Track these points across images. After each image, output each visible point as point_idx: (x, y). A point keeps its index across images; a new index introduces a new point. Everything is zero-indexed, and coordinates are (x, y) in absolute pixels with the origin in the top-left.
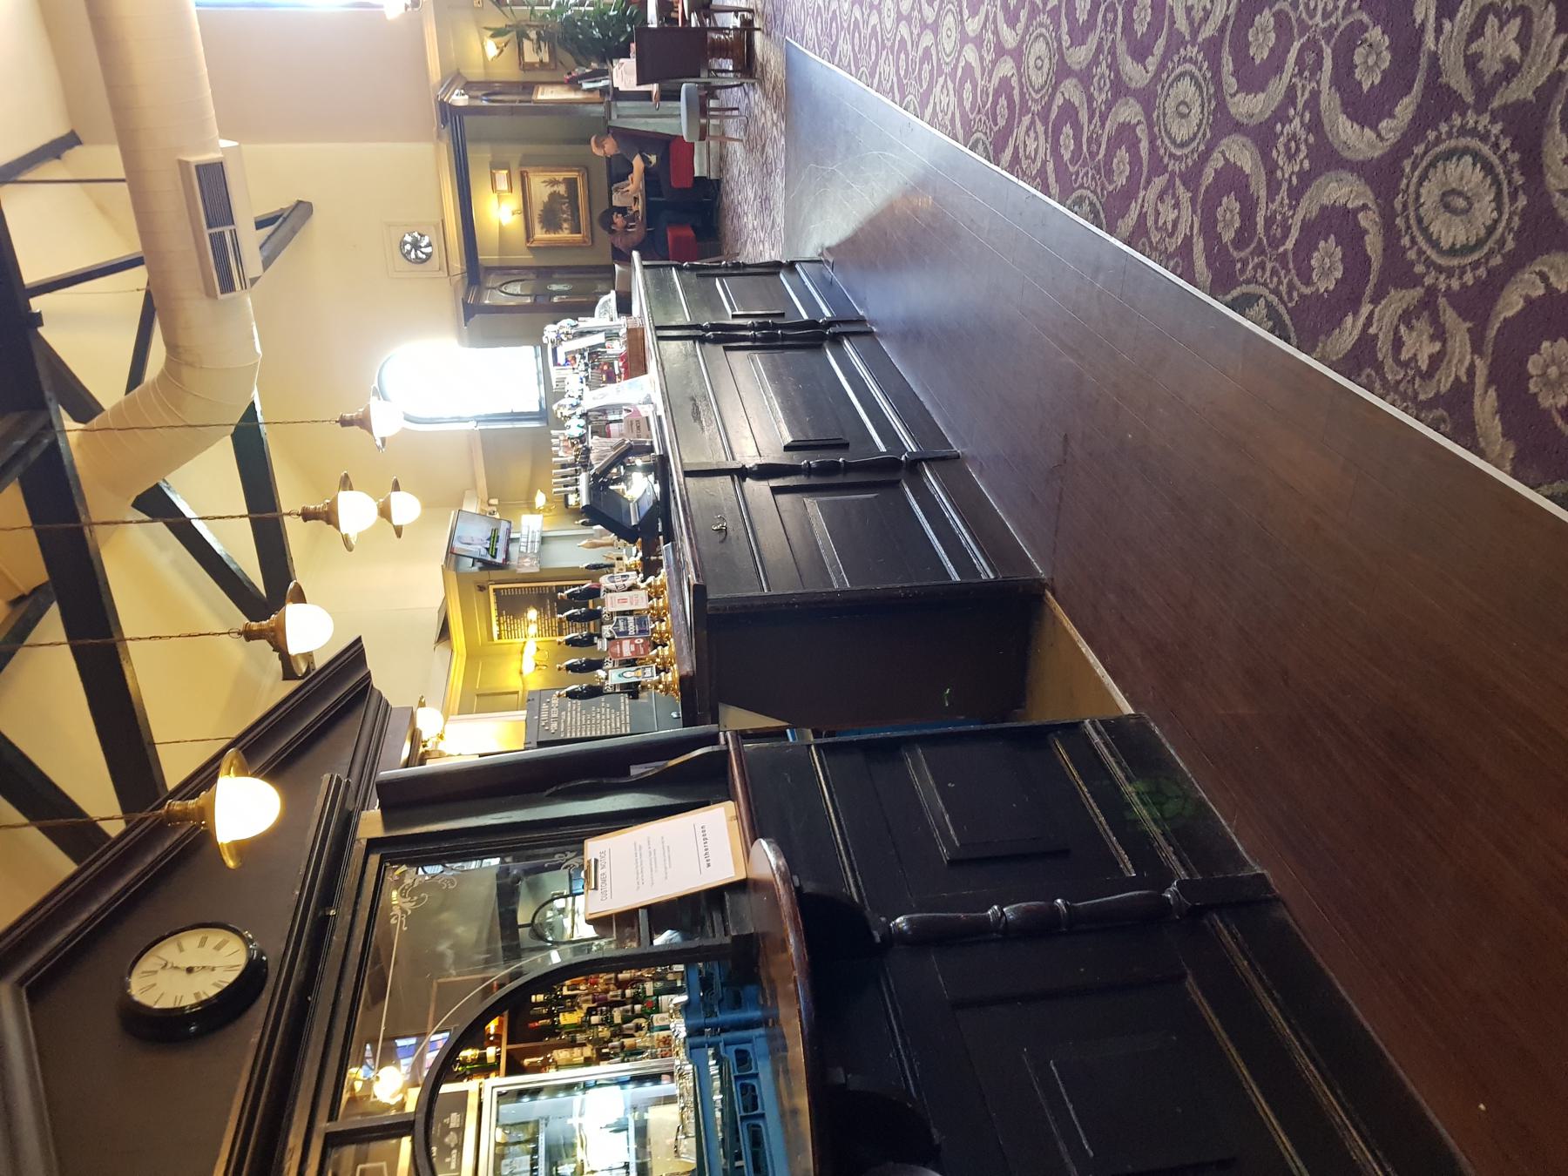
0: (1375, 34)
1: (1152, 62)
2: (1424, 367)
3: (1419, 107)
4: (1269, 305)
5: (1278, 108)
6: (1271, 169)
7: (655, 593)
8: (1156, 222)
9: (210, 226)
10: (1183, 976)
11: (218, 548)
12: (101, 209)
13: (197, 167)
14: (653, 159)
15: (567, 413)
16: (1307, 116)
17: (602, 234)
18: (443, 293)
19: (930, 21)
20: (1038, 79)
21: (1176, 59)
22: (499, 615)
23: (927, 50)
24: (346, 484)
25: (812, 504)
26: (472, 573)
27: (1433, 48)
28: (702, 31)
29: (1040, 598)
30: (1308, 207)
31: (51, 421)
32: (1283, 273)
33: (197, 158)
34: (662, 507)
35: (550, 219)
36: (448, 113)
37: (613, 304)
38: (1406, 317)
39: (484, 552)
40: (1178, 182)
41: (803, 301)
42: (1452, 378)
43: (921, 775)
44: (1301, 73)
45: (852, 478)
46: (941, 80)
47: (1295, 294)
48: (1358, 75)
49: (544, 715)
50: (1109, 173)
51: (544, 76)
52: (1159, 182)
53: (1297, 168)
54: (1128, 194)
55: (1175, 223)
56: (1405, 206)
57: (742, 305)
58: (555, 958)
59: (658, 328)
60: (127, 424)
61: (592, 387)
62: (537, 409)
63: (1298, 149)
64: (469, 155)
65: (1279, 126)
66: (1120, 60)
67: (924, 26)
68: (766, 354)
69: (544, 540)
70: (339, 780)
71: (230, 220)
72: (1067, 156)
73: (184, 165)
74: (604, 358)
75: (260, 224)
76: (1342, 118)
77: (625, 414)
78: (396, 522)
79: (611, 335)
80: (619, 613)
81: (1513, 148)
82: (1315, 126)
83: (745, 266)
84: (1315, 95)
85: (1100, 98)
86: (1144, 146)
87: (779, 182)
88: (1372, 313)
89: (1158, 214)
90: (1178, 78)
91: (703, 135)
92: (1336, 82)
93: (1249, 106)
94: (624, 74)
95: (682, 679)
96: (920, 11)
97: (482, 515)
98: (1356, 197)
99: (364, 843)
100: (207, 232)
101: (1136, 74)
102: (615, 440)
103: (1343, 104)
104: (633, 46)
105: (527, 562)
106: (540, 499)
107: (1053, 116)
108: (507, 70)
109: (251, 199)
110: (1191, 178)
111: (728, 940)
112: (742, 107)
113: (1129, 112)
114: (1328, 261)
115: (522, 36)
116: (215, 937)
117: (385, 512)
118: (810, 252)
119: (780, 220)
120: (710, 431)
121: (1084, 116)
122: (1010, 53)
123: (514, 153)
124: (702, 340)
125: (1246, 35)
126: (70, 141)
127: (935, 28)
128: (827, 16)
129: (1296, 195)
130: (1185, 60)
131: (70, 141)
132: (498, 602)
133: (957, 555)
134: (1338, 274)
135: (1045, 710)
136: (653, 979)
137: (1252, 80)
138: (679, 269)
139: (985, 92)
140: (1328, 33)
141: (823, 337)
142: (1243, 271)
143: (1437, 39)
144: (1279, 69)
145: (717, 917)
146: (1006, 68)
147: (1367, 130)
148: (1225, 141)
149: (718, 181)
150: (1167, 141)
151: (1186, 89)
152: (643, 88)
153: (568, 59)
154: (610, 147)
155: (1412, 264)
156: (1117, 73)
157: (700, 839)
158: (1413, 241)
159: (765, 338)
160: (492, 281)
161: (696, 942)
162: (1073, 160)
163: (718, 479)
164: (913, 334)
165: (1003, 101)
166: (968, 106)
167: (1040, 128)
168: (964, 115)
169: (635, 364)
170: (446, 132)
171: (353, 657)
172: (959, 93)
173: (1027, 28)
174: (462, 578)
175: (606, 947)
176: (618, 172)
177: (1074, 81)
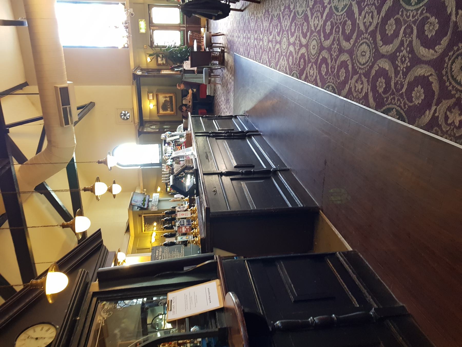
0: (432, 19)
1: (352, 41)
2: (457, 125)
3: (450, 40)
4: (397, 111)
5: (397, 48)
6: (396, 67)
7: (193, 212)
8: (355, 89)
9: (63, 106)
10: (380, 343)
11: (60, 203)
12: (33, 104)
13: (60, 88)
14: (195, 90)
15: (167, 158)
16: (408, 49)
17: (179, 112)
18: (132, 129)
20: (313, 52)
21: (360, 39)
22: (145, 224)
23: (278, 49)
24: (98, 180)
25: (243, 184)
26: (137, 211)
27: (455, 20)
28: (210, 53)
29: (318, 213)
30: (410, 77)
31: (9, 162)
32: (401, 100)
33: (59, 86)
34: (196, 187)
35: (165, 107)
36: (135, 77)
37: (182, 128)
39: (141, 204)
40: (362, 76)
41: (238, 126)
43: (283, 271)
44: (405, 36)
45: (255, 176)
46: (282, 57)
47: (407, 106)
48: (426, 33)
49: (157, 254)
50: (338, 77)
51: (164, 67)
52: (356, 77)
53: (405, 66)
54: (345, 82)
55: (362, 89)
56: (447, 72)
57: (221, 126)
58: (159, 335)
59: (195, 133)
60: (34, 163)
61: (175, 150)
62: (159, 162)
63: (405, 60)
64: (142, 89)
65: (398, 54)
66: (341, 42)
67: (277, 42)
68: (228, 141)
69: (159, 201)
70: (84, 272)
71: (69, 104)
72: (324, 74)
73: (56, 88)
74: (179, 143)
75: (78, 108)
76: (421, 48)
77: (185, 158)
78: (114, 193)
79: (181, 136)
80: (182, 218)
82: (412, 51)
83: (222, 116)
84: (411, 42)
86: (350, 67)
87: (232, 94)
88: (436, 109)
89: (355, 87)
90: (361, 44)
91: (210, 82)
92: (418, 36)
93: (386, 49)
94: (187, 65)
95: (201, 239)
96: (275, 38)
97: (141, 193)
98: (428, 72)
99: (92, 293)
100: (62, 107)
101: (346, 45)
102: (181, 165)
103: (421, 43)
104: (190, 57)
105: (154, 208)
106: (159, 189)
107: (319, 62)
108: (153, 66)
109: (77, 100)
110: (367, 75)
111: (217, 330)
112: (221, 75)
113: (345, 57)
114: (418, 95)
115: (158, 56)
116: (46, 327)
117: (110, 190)
118: (241, 113)
119: (232, 105)
120: (212, 162)
121: (329, 61)
122: (304, 46)
123: (155, 88)
124: (209, 136)
125: (385, 28)
126: (26, 84)
127: (280, 43)
128: (246, 45)
129: (405, 75)
130: (364, 39)
131: (26, 84)
132: (145, 220)
133: (290, 198)
134: (423, 98)
135: (321, 248)
136: (190, 343)
137: (387, 40)
138: (202, 117)
139: (296, 59)
140: (414, 22)
141: (246, 136)
142: (387, 101)
143: (456, 17)
144: (397, 36)
145: (213, 321)
146: (303, 50)
147: (431, 50)
148: (379, 61)
149: (214, 96)
150: (358, 64)
151: (364, 47)
152: (192, 69)
153: (171, 62)
154: (182, 87)
155: (451, 91)
156: (340, 46)
157: (207, 292)
158: (450, 83)
159: (228, 136)
160: (147, 125)
161: (205, 331)
163: (214, 176)
164: (273, 135)
165: (302, 60)
166: (291, 63)
167: (315, 67)
168: (289, 66)
169: (188, 144)
170: (135, 82)
171: (98, 235)
172: (288, 60)
173: (310, 38)
174: (134, 213)
175: (175, 332)
176: (185, 94)
177: (326, 51)
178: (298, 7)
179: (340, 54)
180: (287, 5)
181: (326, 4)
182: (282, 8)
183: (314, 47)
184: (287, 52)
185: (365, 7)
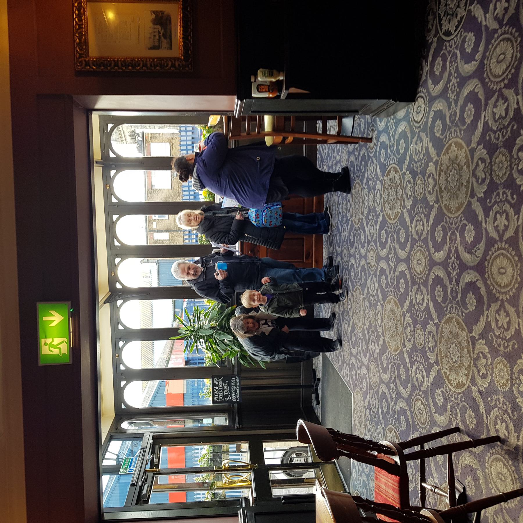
1: (407, 249)
16: (455, 255)
19: (363, 255)
20: (419, 269)
30: (462, 285)
38: (498, 312)
40: (506, 303)
42: (514, 329)
47: (464, 314)
63: (455, 266)
65: (449, 261)
72: (384, 286)
81: (513, 250)
82: (458, 258)
85: (454, 273)
86: (483, 291)
89: (416, 299)
101: (402, 254)
113: (402, 267)
114: (471, 300)
121: (388, 272)
137: (438, 248)
151: (420, 255)
162: (386, 287)
167: (375, 279)
178: (354, 215)
179: (397, 263)
180: (344, 214)
181: (378, 213)
182: (366, 212)
183: (419, 262)
184: (377, 270)
185: (415, 215)
